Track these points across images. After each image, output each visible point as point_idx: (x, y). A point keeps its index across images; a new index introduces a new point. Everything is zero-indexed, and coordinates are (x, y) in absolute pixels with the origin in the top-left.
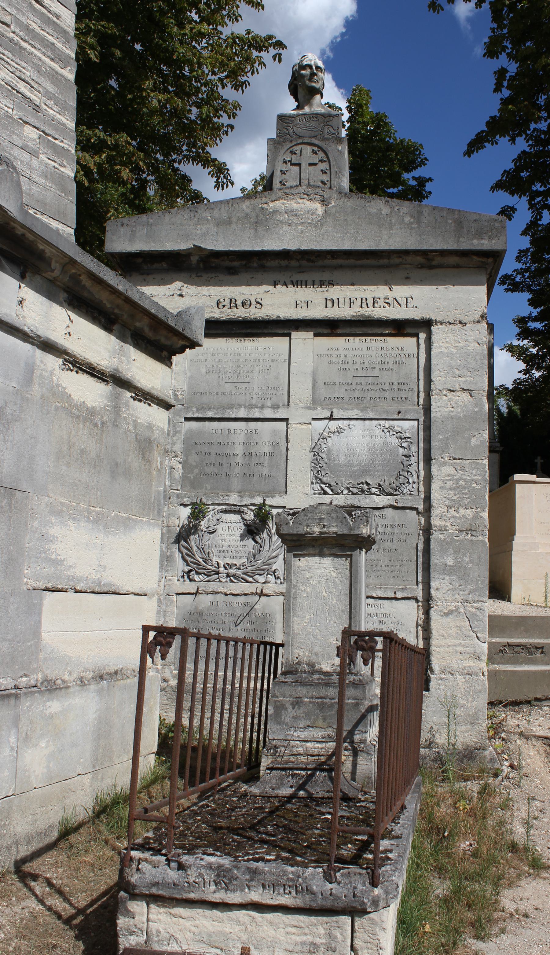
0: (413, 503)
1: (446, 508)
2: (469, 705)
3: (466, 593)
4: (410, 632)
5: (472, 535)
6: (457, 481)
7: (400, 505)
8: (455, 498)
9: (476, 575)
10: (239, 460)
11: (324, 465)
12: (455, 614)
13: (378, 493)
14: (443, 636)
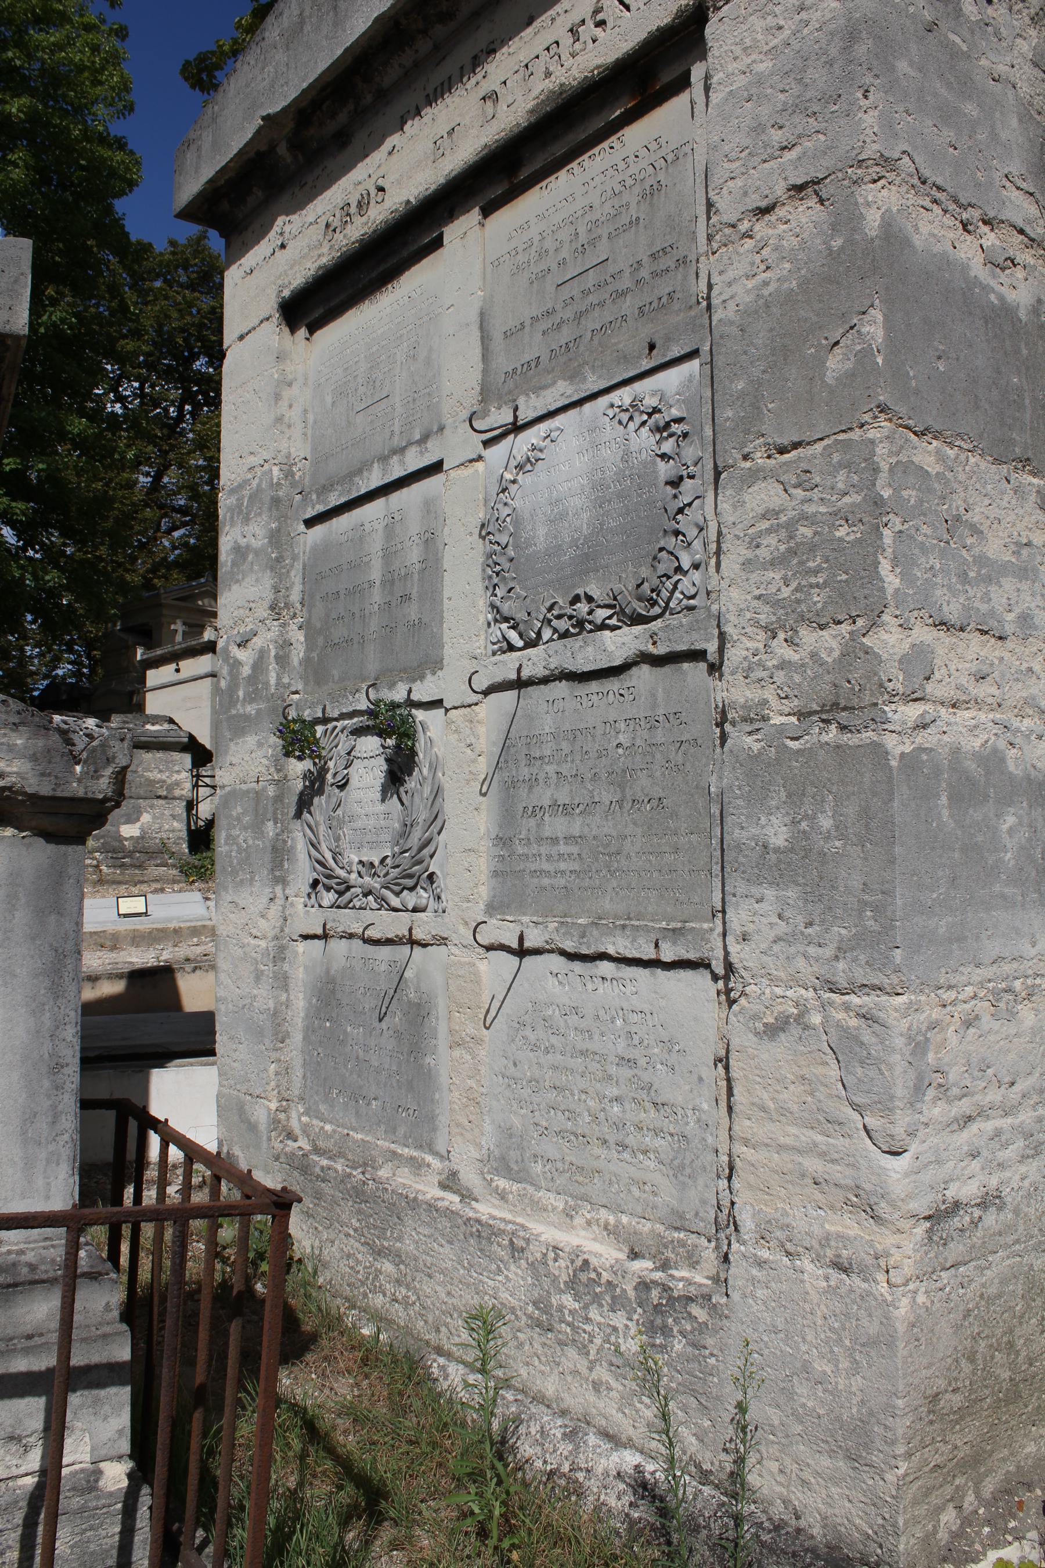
0: (695, 635)
1: (762, 636)
2: (842, 1383)
3: (829, 952)
4: (701, 1079)
5: (843, 728)
6: (790, 527)
7: (661, 650)
8: (786, 592)
9: (856, 883)
10: (377, 596)
11: (507, 565)
12: (795, 1030)
13: (613, 621)
14: (763, 1109)
